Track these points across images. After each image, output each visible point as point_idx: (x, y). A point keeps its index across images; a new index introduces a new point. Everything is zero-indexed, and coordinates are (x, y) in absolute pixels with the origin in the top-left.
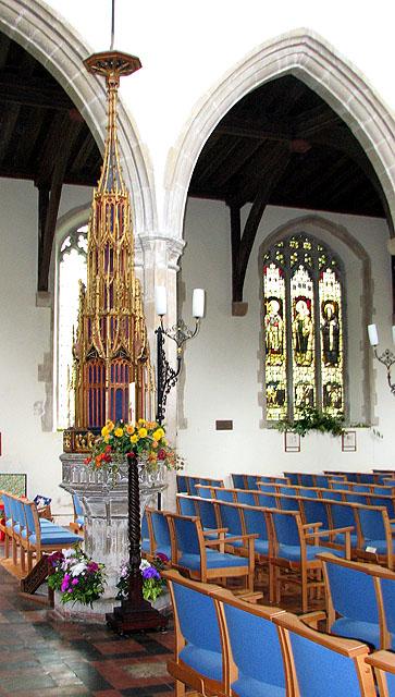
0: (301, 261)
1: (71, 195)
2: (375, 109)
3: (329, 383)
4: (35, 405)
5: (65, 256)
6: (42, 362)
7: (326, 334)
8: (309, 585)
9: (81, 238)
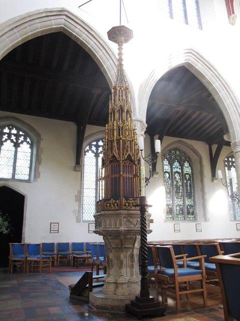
0: (176, 158)
1: (90, 129)
2: (219, 80)
3: (189, 205)
4: (74, 211)
5: (87, 153)
6: (77, 194)
7: (187, 186)
8: (180, 293)
9: (93, 146)
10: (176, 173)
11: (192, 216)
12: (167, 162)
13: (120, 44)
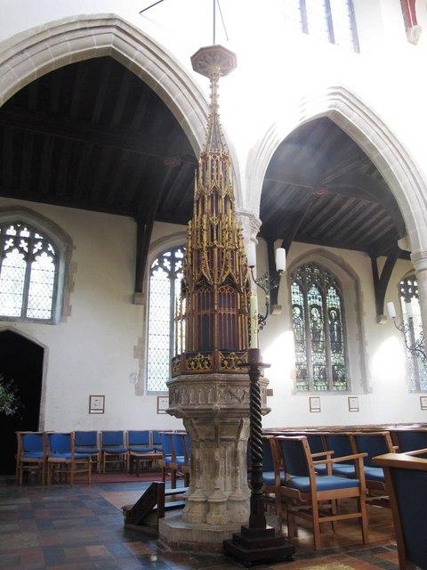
0: (313, 281)
1: (160, 230)
2: (390, 141)
3: (336, 364)
4: (131, 375)
5: (154, 272)
6: (137, 344)
7: (332, 330)
8: (321, 520)
9: (165, 260)
10: (312, 306)
11: (342, 384)
12: (298, 287)
13: (213, 78)
